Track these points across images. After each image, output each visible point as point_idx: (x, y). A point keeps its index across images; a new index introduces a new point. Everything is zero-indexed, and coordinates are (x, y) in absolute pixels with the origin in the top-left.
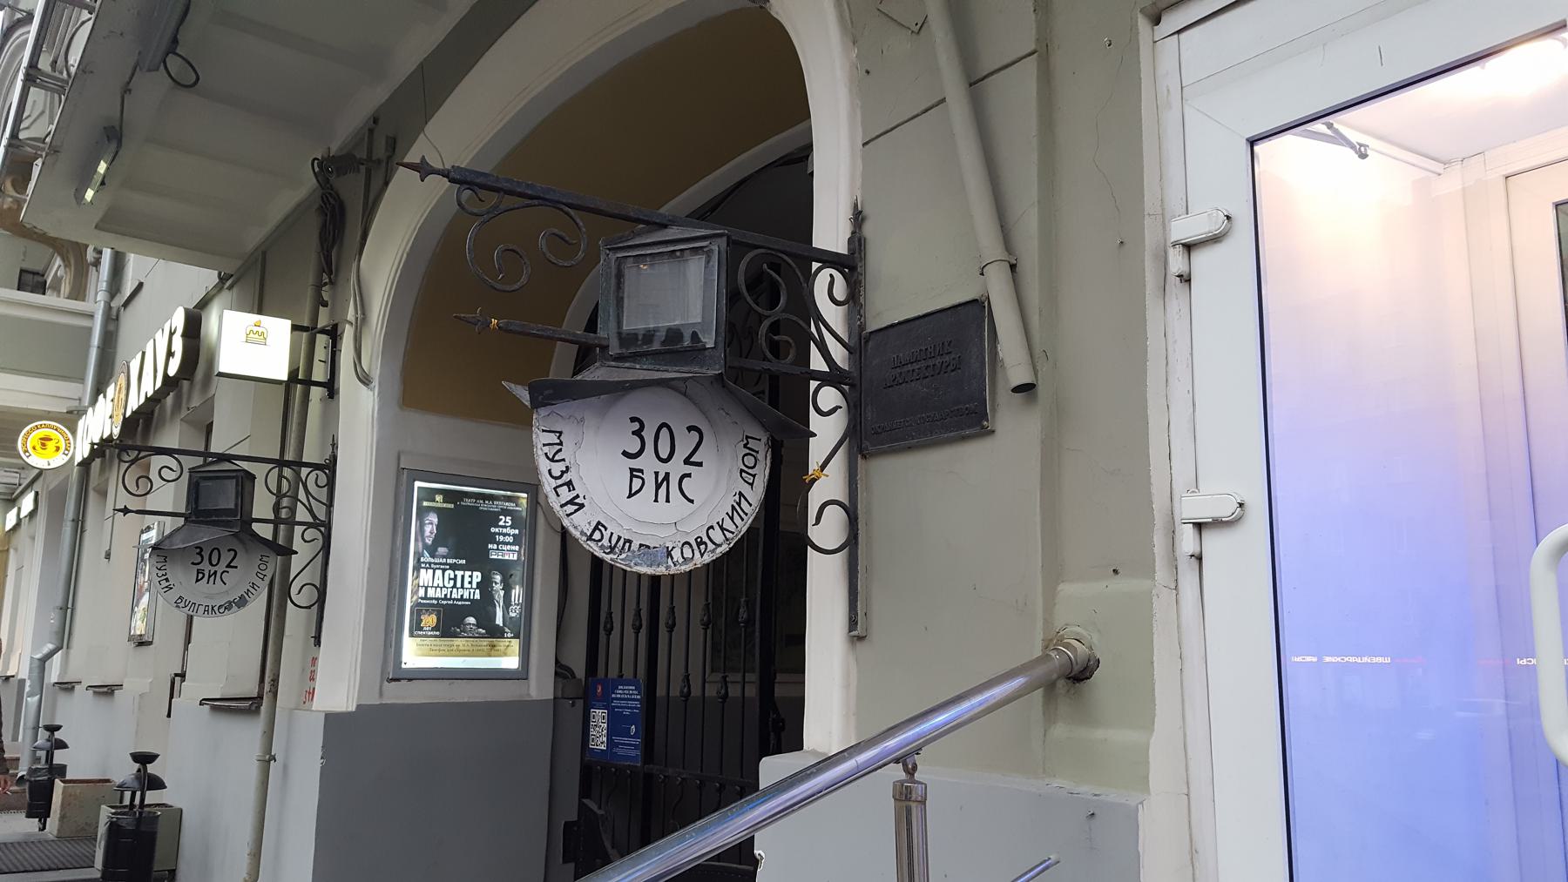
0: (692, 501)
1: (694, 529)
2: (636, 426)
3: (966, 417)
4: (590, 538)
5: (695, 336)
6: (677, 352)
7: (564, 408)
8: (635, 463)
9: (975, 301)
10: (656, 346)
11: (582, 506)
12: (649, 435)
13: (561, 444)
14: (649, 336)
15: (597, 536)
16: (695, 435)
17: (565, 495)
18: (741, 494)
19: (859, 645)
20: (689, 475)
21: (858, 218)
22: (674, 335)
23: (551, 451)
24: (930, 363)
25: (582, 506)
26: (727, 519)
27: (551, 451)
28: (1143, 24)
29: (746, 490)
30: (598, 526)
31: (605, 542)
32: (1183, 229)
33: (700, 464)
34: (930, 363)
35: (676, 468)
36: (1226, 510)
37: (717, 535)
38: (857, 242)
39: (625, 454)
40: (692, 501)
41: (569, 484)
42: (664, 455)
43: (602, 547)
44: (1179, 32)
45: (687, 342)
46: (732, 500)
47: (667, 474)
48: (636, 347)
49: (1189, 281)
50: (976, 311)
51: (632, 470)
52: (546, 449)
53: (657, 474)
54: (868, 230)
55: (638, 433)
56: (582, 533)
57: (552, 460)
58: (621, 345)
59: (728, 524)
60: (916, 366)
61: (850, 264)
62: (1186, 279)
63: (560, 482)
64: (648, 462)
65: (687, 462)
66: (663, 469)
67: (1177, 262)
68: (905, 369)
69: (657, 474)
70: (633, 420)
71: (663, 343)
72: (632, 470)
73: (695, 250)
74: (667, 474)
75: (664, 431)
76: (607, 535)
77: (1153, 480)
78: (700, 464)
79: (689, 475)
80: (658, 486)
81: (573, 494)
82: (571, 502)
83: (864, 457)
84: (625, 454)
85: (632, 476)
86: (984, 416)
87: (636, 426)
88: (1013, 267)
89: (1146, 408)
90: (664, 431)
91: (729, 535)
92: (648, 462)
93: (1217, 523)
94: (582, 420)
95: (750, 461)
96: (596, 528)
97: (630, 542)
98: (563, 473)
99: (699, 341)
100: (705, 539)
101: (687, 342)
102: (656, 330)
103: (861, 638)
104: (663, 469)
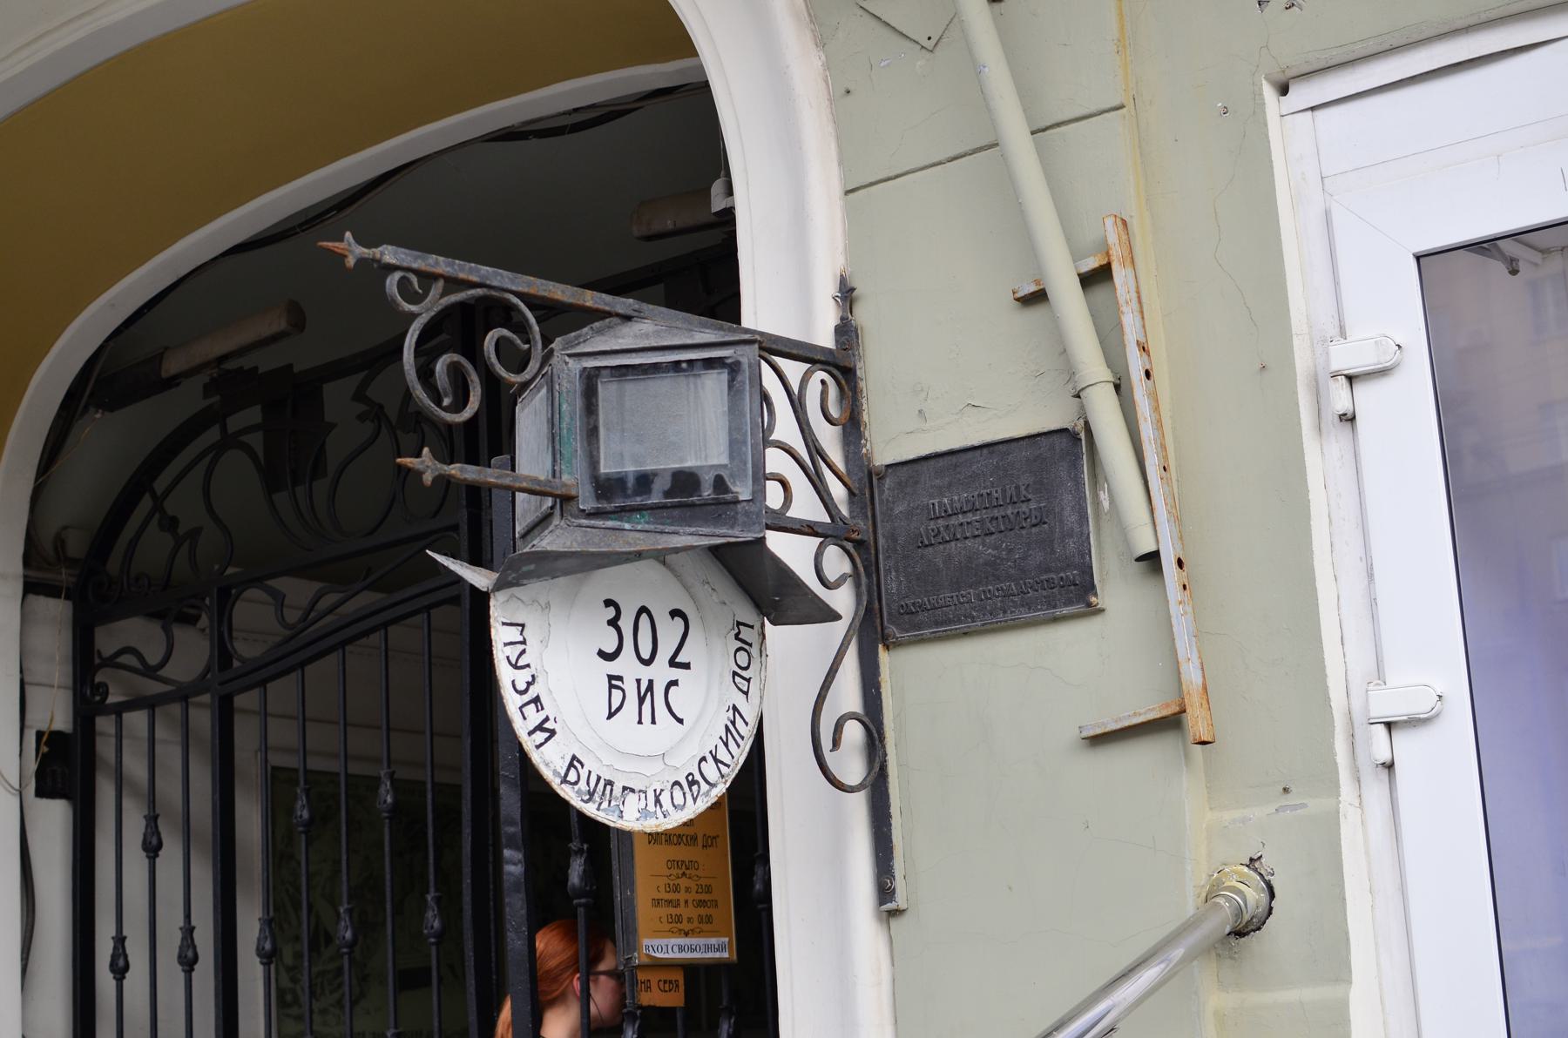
0: (681, 721)
1: (685, 764)
2: (611, 613)
3: (1057, 585)
4: (564, 780)
5: (720, 484)
6: (693, 505)
7: (534, 588)
8: (614, 667)
9: (1066, 430)
10: (655, 498)
11: (552, 733)
12: (626, 624)
13: (524, 642)
14: (644, 481)
15: (572, 777)
16: (679, 621)
17: (534, 717)
18: (735, 708)
19: (894, 923)
20: (674, 683)
21: (847, 295)
22: (685, 481)
23: (513, 652)
24: (996, 513)
25: (552, 733)
26: (721, 747)
27: (513, 652)
28: (1269, 93)
29: (739, 701)
30: (574, 762)
31: (582, 785)
32: (1347, 358)
33: (686, 666)
34: (996, 513)
35: (660, 672)
36: (1420, 708)
37: (710, 769)
38: (846, 331)
39: (602, 654)
40: (681, 721)
41: (536, 700)
42: (646, 655)
43: (579, 792)
44: (1312, 109)
45: (707, 492)
46: (725, 717)
47: (651, 682)
48: (617, 495)
49: (1352, 419)
50: (1071, 446)
51: (611, 678)
52: (509, 650)
53: (638, 681)
54: (863, 315)
55: (613, 623)
56: (556, 773)
57: (516, 667)
58: (598, 498)
59: (723, 754)
60: (970, 517)
61: (840, 365)
62: (1349, 419)
63: (526, 698)
64: (626, 665)
65: (673, 663)
66: (645, 673)
67: (1340, 399)
68: (954, 521)
69: (638, 681)
70: (609, 603)
71: (668, 494)
72: (611, 678)
73: (709, 363)
74: (651, 682)
75: (644, 617)
76: (584, 774)
77: (1328, 671)
78: (686, 666)
79: (674, 683)
80: (641, 700)
81: (542, 715)
82: (540, 728)
83: (887, 648)
84: (602, 654)
85: (611, 687)
86: (1091, 588)
87: (611, 613)
88: (1117, 387)
89: (1314, 580)
90: (644, 617)
91: (724, 769)
92: (626, 665)
93: (1414, 722)
94: (548, 605)
95: (742, 658)
96: (571, 765)
97: (610, 783)
98: (529, 684)
99: (727, 490)
100: (698, 777)
101: (707, 492)
102: (655, 474)
103: (895, 913)
104: (645, 673)
